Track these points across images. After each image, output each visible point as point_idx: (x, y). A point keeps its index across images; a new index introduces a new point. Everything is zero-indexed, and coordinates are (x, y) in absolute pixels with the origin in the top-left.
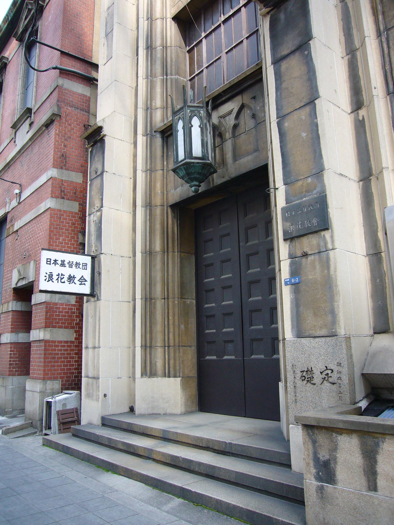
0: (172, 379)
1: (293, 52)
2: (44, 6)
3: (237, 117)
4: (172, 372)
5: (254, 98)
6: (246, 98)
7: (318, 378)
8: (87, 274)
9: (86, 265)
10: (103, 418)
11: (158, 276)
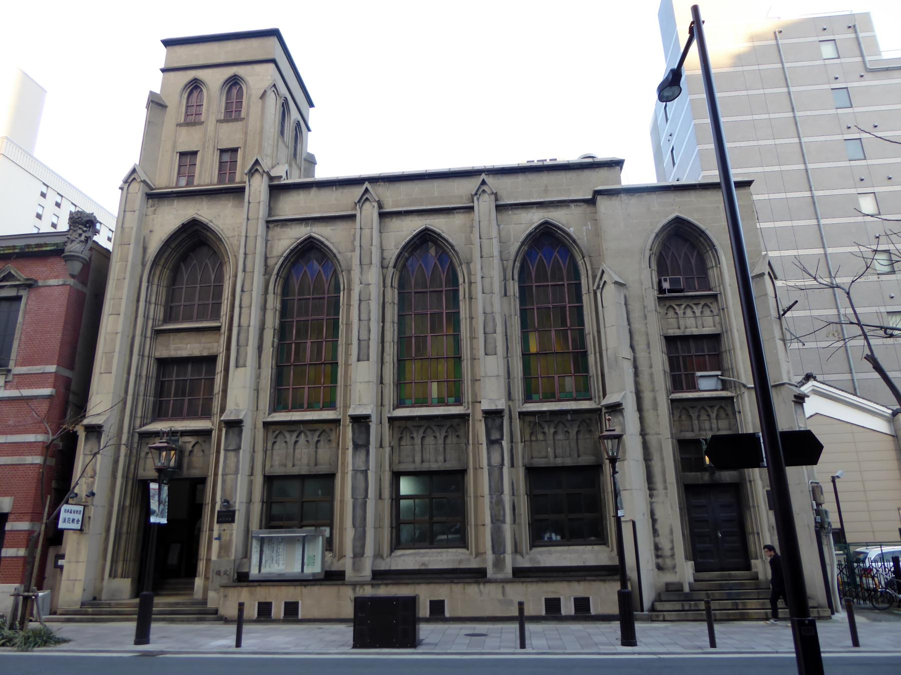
0: (126, 579)
1: (232, 450)
2: (218, 522)
3: (193, 447)
4: (126, 576)
5: (205, 441)
6: (200, 440)
7: (222, 573)
8: (80, 517)
9: (80, 511)
10: (664, 489)
11: (126, 520)
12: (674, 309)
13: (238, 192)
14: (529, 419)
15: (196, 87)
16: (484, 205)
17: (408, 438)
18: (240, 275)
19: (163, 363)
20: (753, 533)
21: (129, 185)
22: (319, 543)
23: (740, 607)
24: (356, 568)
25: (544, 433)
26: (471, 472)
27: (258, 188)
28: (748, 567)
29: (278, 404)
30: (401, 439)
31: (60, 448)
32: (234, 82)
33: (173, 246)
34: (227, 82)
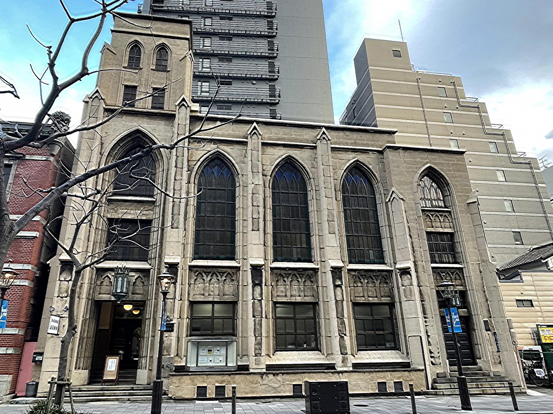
12: (439, 217)
13: (170, 117)
14: (276, 271)
15: (136, 46)
16: (254, 142)
17: (282, 280)
18: (173, 170)
19: (111, 221)
20: (477, 344)
21: (93, 100)
22: (233, 347)
23: (480, 387)
24: (258, 363)
25: (361, 283)
26: (321, 304)
27: (183, 116)
28: (476, 364)
29: (197, 255)
30: (277, 281)
31: (37, 275)
32: (162, 48)
33: (121, 145)
34: (158, 46)
